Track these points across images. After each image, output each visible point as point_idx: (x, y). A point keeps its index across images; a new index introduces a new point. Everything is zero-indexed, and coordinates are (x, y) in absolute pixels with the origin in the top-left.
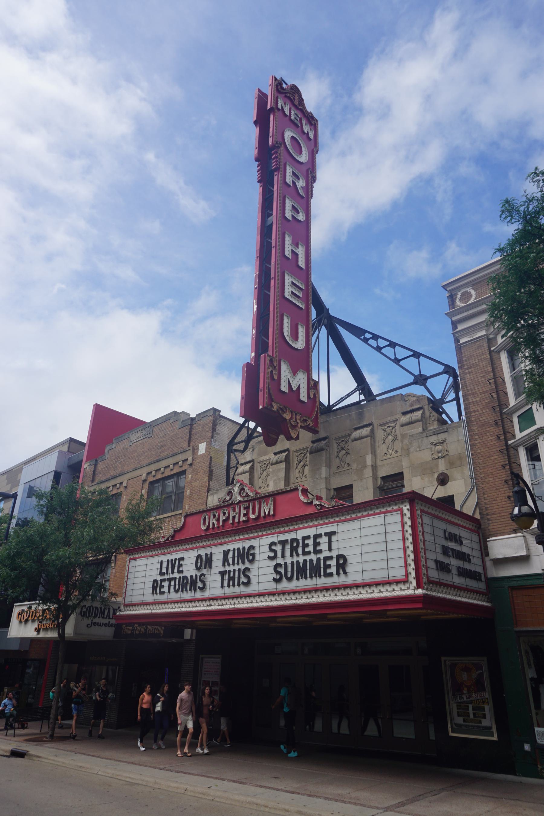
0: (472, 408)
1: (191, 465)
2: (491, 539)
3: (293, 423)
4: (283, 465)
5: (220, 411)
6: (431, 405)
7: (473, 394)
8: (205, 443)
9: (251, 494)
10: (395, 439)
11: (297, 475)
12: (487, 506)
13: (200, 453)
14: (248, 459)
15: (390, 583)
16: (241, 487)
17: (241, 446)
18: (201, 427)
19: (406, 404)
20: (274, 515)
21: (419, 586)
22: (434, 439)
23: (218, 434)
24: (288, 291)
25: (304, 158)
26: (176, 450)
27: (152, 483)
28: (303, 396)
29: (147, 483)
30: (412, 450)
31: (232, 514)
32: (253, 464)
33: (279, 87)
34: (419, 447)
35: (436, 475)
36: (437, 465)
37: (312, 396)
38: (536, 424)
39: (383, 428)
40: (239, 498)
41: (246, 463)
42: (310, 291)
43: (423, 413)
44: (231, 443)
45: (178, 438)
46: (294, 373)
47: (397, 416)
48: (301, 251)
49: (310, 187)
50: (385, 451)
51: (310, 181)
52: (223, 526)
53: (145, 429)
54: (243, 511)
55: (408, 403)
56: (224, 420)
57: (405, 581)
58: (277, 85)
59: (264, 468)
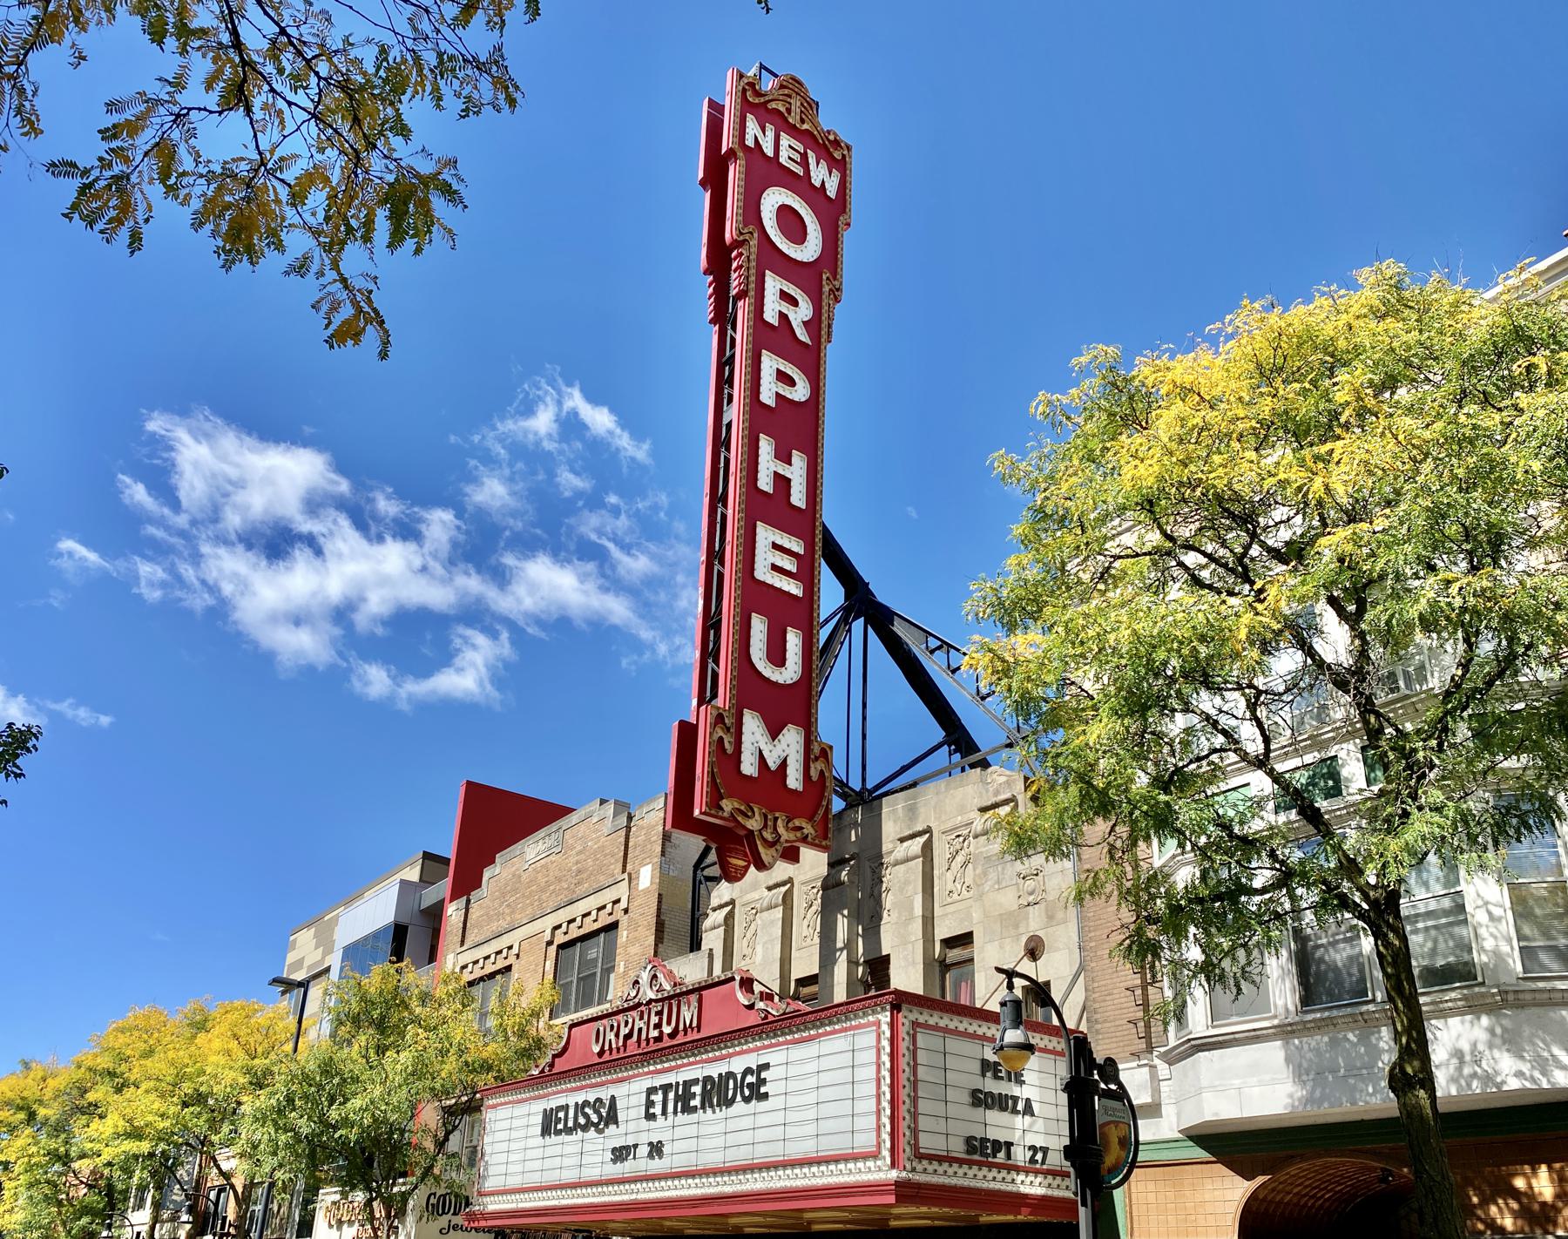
1: (626, 911)
9: (668, 987)
13: (641, 887)
14: (726, 899)
15: (855, 1158)
21: (893, 1165)
24: (764, 559)
27: (562, 947)
28: (794, 780)
29: (553, 948)
32: (930, 840)
34: (998, 882)
35: (1024, 939)
37: (814, 774)
40: (651, 995)
41: (721, 907)
44: (698, 866)
46: (774, 732)
48: (797, 471)
57: (875, 1156)
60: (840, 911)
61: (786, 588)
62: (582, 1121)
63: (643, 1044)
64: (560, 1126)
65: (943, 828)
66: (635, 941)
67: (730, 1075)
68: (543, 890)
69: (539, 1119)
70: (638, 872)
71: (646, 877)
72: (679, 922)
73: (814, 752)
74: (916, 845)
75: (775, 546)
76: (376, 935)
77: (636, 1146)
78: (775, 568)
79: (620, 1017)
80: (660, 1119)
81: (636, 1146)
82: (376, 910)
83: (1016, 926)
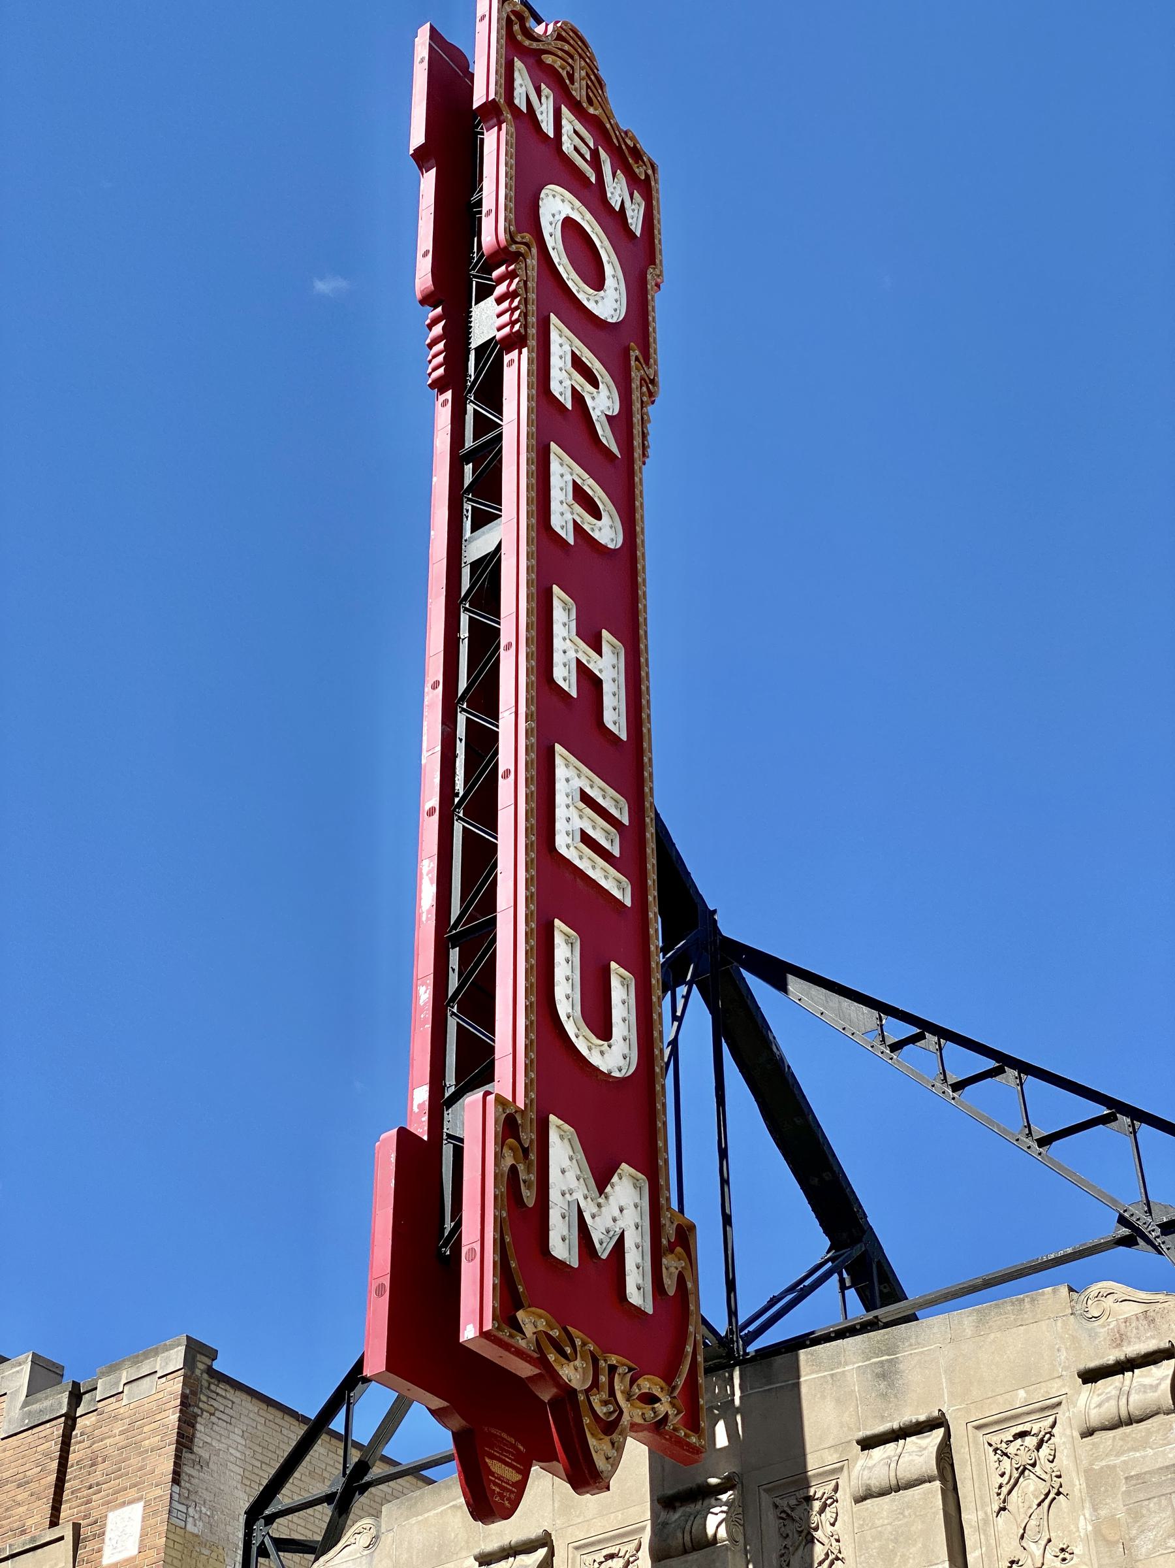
3: (601, 1410)
5: (213, 1354)
8: (138, 1507)
10: (1052, 1495)
18: (118, 1427)
19: (1093, 1335)
23: (201, 1464)
24: (570, 820)
25: (609, 304)
33: (516, 28)
39: (995, 1439)
47: (1055, 1389)
48: (609, 665)
49: (637, 418)
51: (636, 395)
55: (1102, 1330)
56: (231, 1394)
58: (509, 23)
61: (609, 885)
65: (976, 1415)
70: (100, 1524)
73: (671, 1238)
74: (919, 1453)
75: (585, 798)
78: (586, 839)
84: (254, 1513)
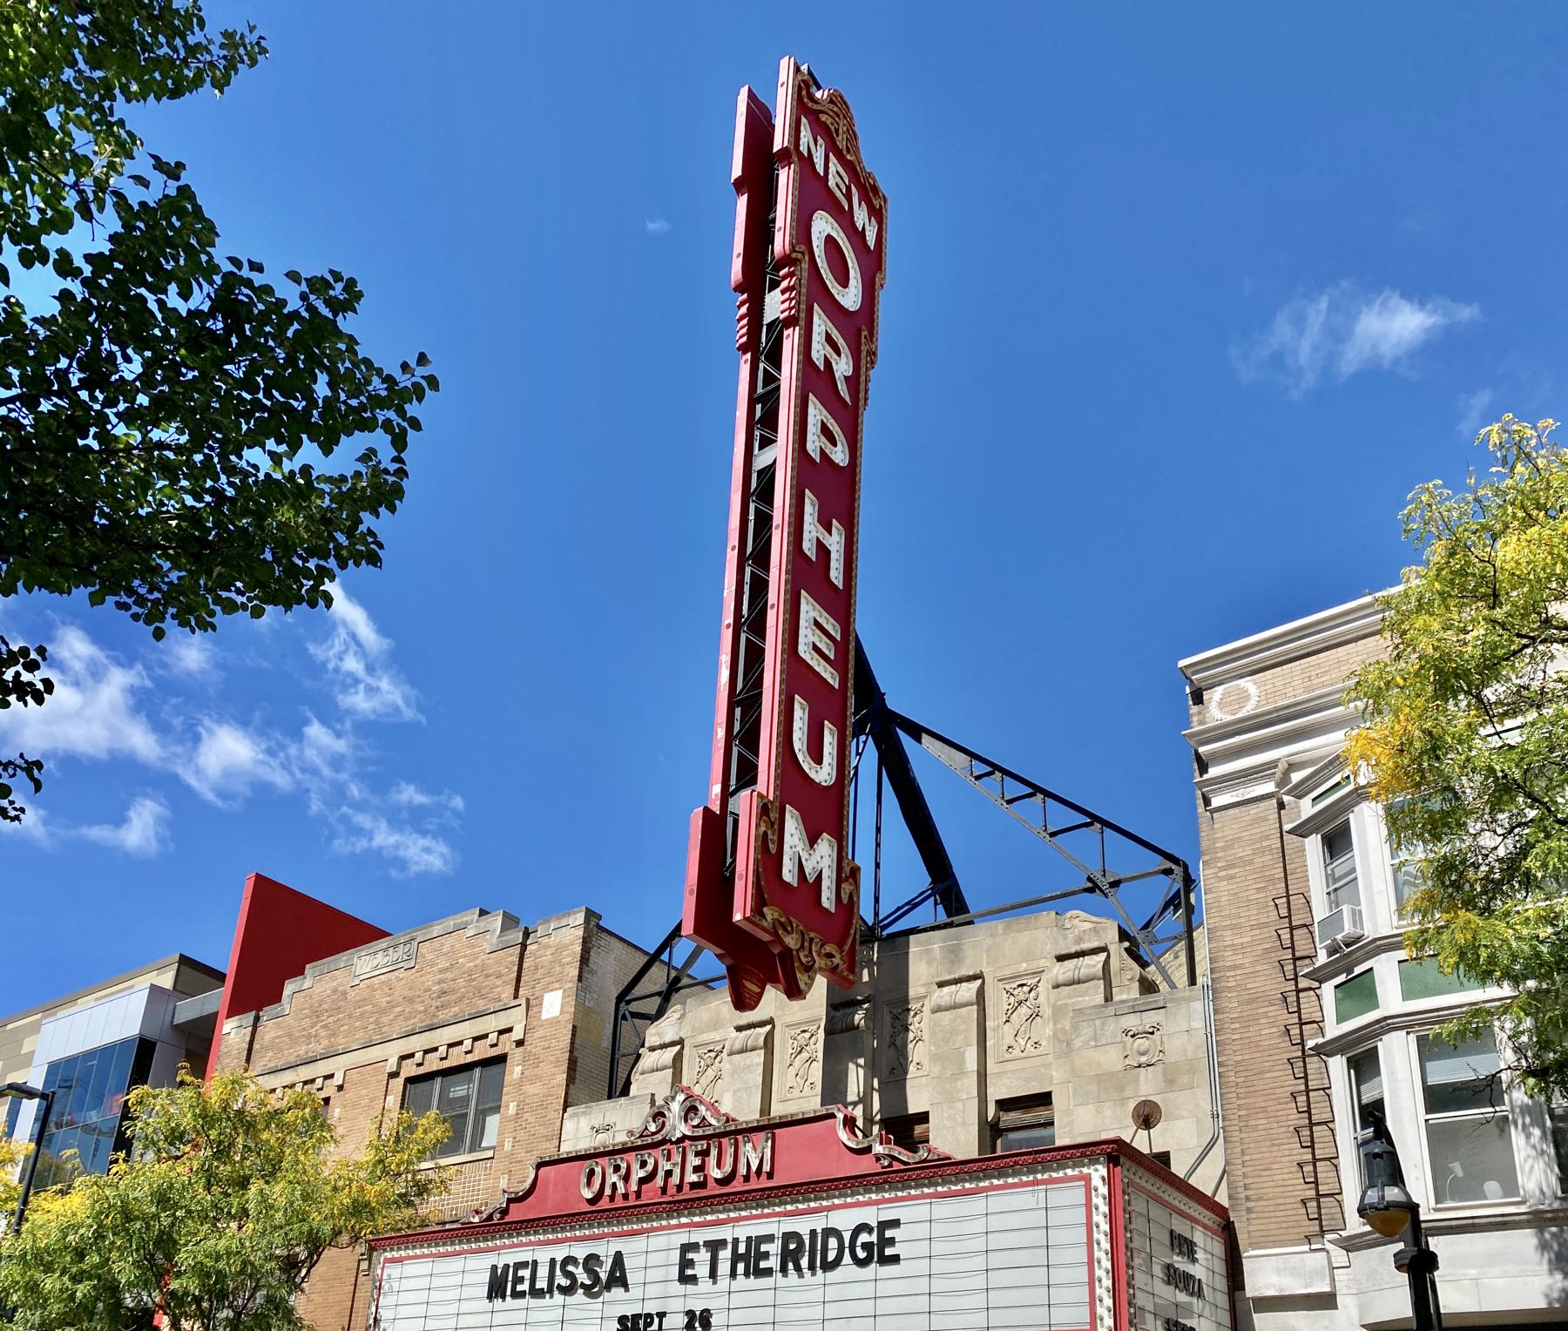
0: (1230, 959)
1: (520, 1043)
2: (1252, 1253)
3: (804, 960)
4: (758, 1057)
6: (1127, 944)
7: (1233, 927)
8: (560, 993)
9: (714, 1122)
11: (791, 1081)
12: (1247, 1181)
13: (544, 1016)
16: (688, 1104)
17: (651, 1006)
19: (1065, 937)
20: (770, 1175)
22: (1132, 1022)
25: (850, 298)
26: (481, 1005)
27: (410, 1081)
28: (827, 899)
29: (400, 1081)
30: (1078, 1043)
31: (665, 1166)
34: (1095, 1039)
35: (1132, 1105)
36: (1136, 1080)
38: (1376, 1006)
40: (683, 1129)
41: (664, 1046)
42: (852, 645)
43: (1107, 963)
45: (487, 976)
46: (812, 841)
47: (1042, 963)
48: (835, 542)
49: (863, 378)
50: (1009, 1040)
51: (863, 363)
52: (638, 1194)
53: (395, 947)
54: (694, 1161)
56: (609, 938)
59: (709, 1061)
60: (853, 1059)
61: (826, 676)
62: (562, 1281)
63: (618, 1198)
64: (525, 1287)
65: (1000, 974)
66: (535, 1077)
67: (829, 1232)
68: (383, 1012)
69: (486, 1277)
71: (555, 1005)
72: (596, 1064)
73: (847, 874)
74: (968, 991)
76: (105, 1052)
77: (661, 1315)
78: (816, 648)
79: (631, 1156)
80: (705, 1285)
81: (661, 1315)
82: (113, 1016)
83: (1121, 1089)
84: (621, 998)
